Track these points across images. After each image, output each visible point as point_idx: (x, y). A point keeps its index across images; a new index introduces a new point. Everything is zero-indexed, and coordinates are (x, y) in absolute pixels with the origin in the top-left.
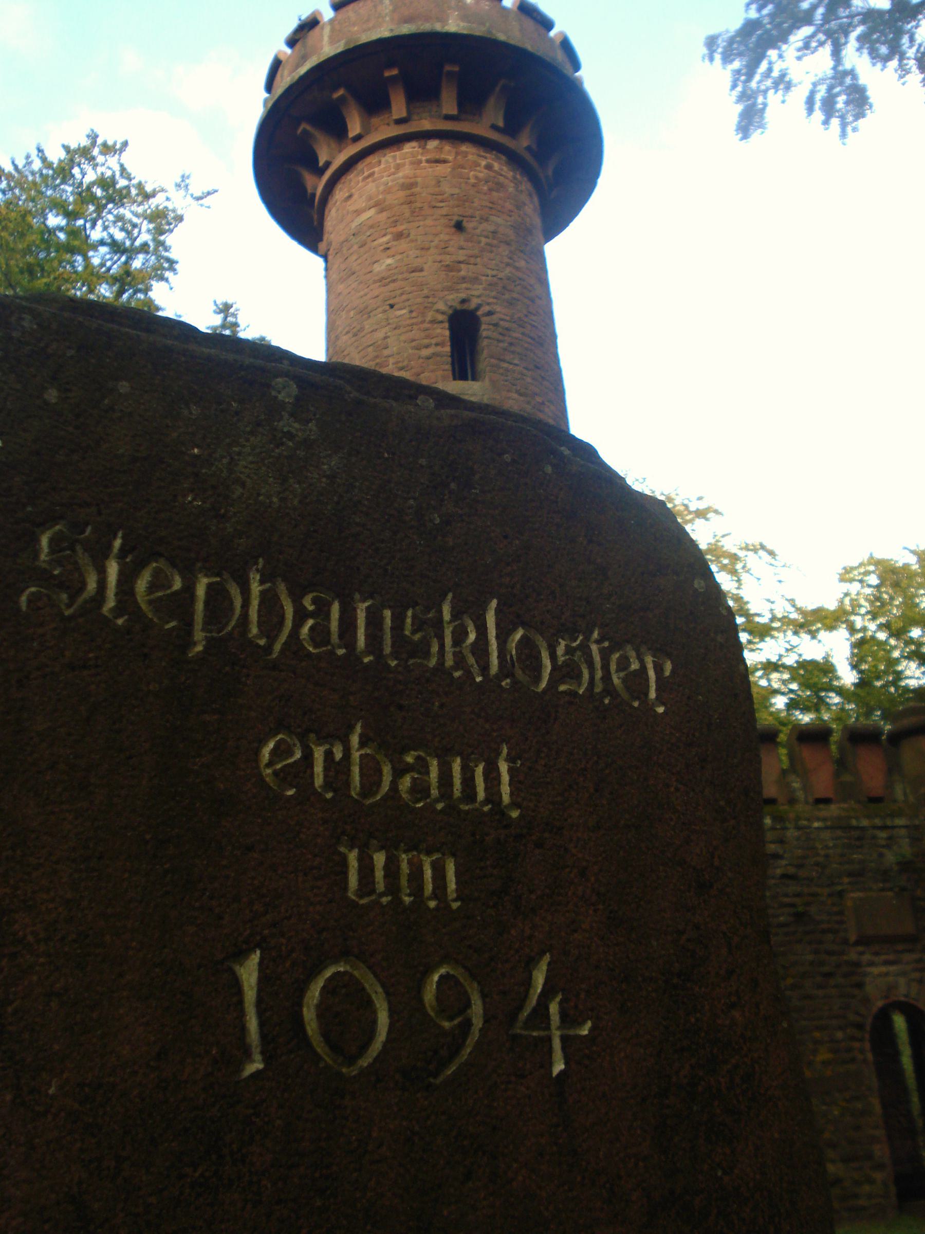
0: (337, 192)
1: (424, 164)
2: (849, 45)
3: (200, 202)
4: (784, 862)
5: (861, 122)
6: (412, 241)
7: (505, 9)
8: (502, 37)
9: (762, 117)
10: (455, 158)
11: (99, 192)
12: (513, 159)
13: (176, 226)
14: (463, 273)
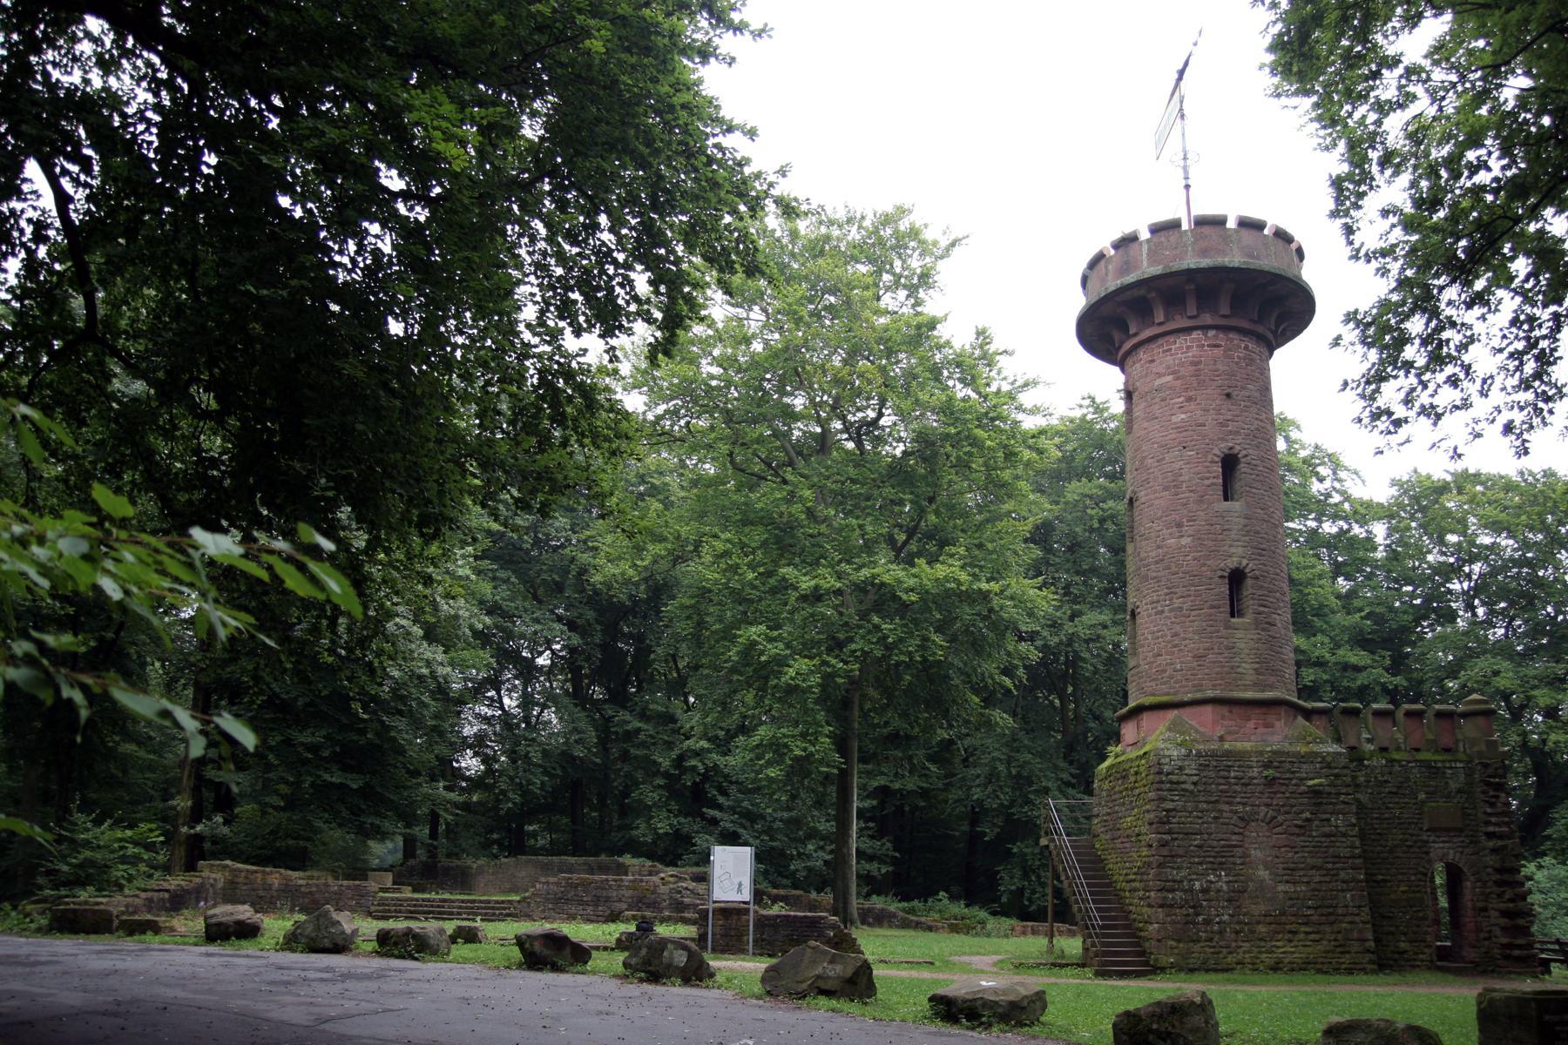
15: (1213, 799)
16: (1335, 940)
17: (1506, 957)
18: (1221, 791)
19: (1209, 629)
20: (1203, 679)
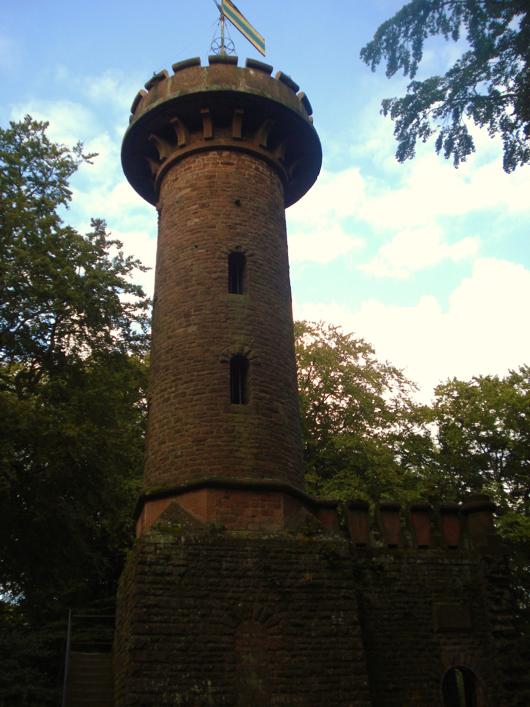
0: (169, 176)
1: (220, 165)
2: (463, 113)
3: (88, 160)
4: (400, 583)
5: (467, 156)
6: (210, 209)
7: (272, 78)
8: (269, 96)
9: (412, 149)
10: (238, 162)
11: (30, 150)
12: (271, 165)
13: (73, 172)
14: (238, 230)
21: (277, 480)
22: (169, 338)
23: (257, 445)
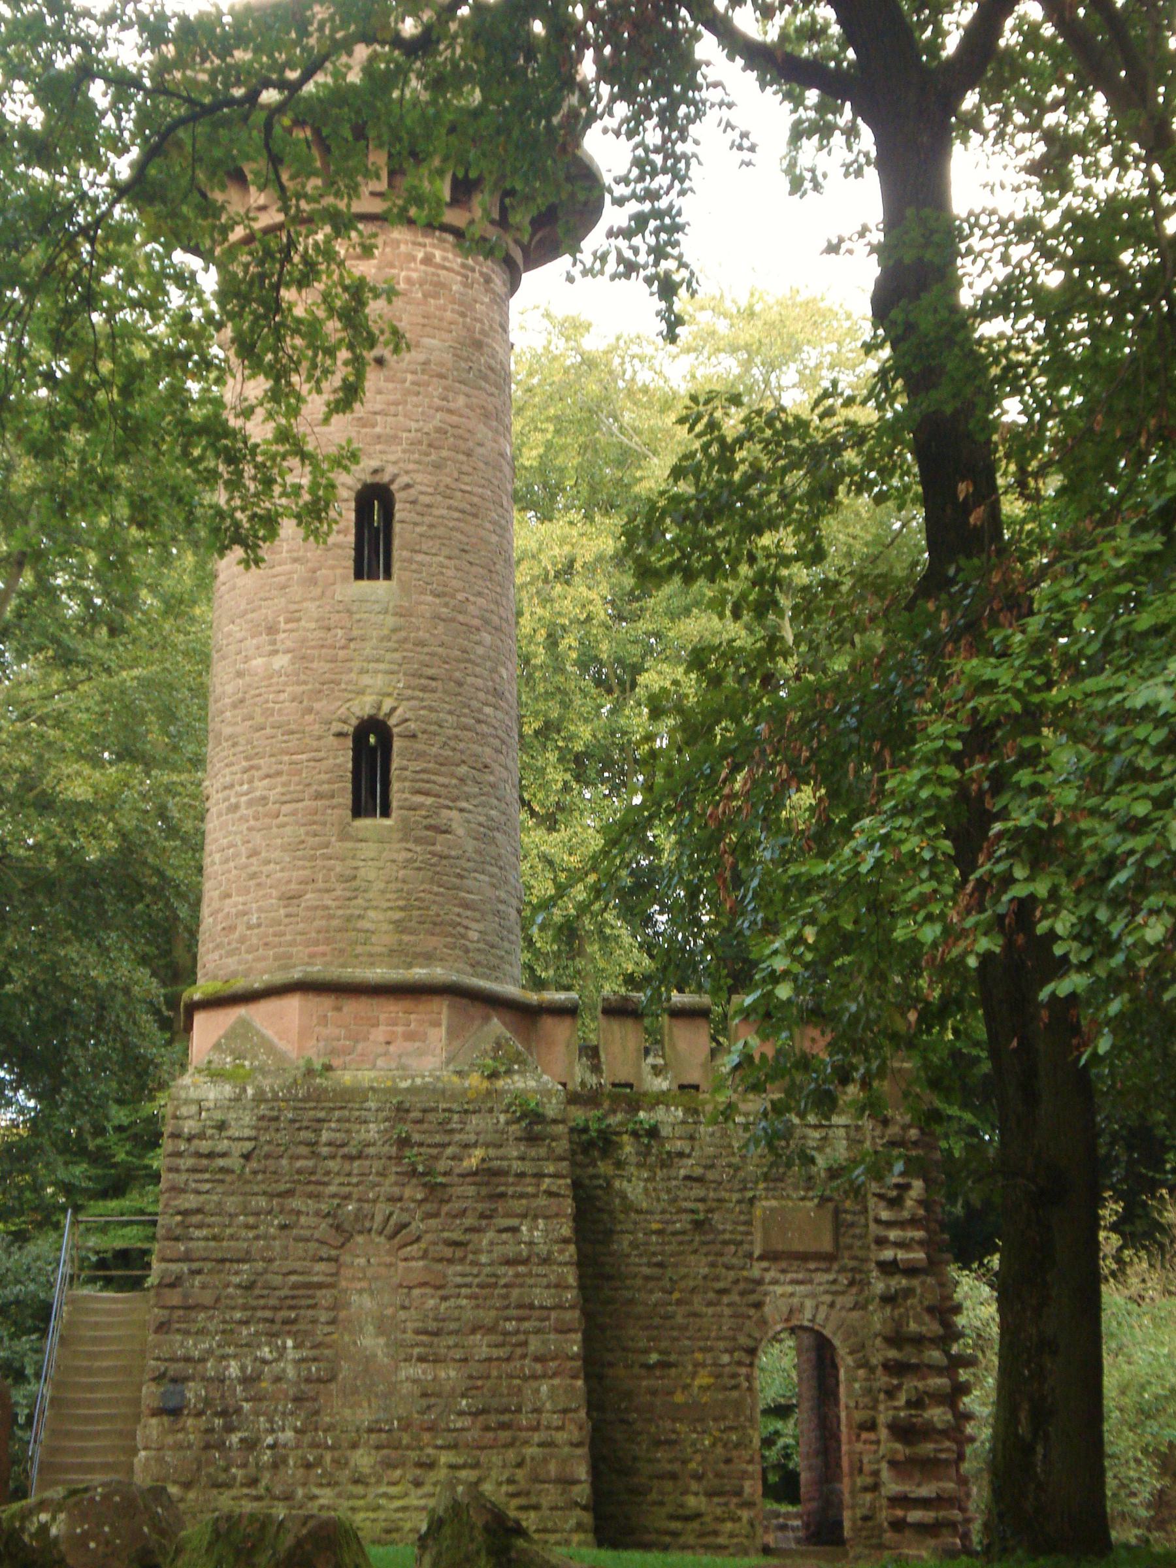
4: (691, 1161)
14: (378, 430)
15: (283, 1187)
16: (511, 1481)
17: (898, 1525)
18: (299, 1172)
19: (312, 841)
20: (292, 944)
21: (438, 973)
22: (240, 674)
23: (401, 903)
